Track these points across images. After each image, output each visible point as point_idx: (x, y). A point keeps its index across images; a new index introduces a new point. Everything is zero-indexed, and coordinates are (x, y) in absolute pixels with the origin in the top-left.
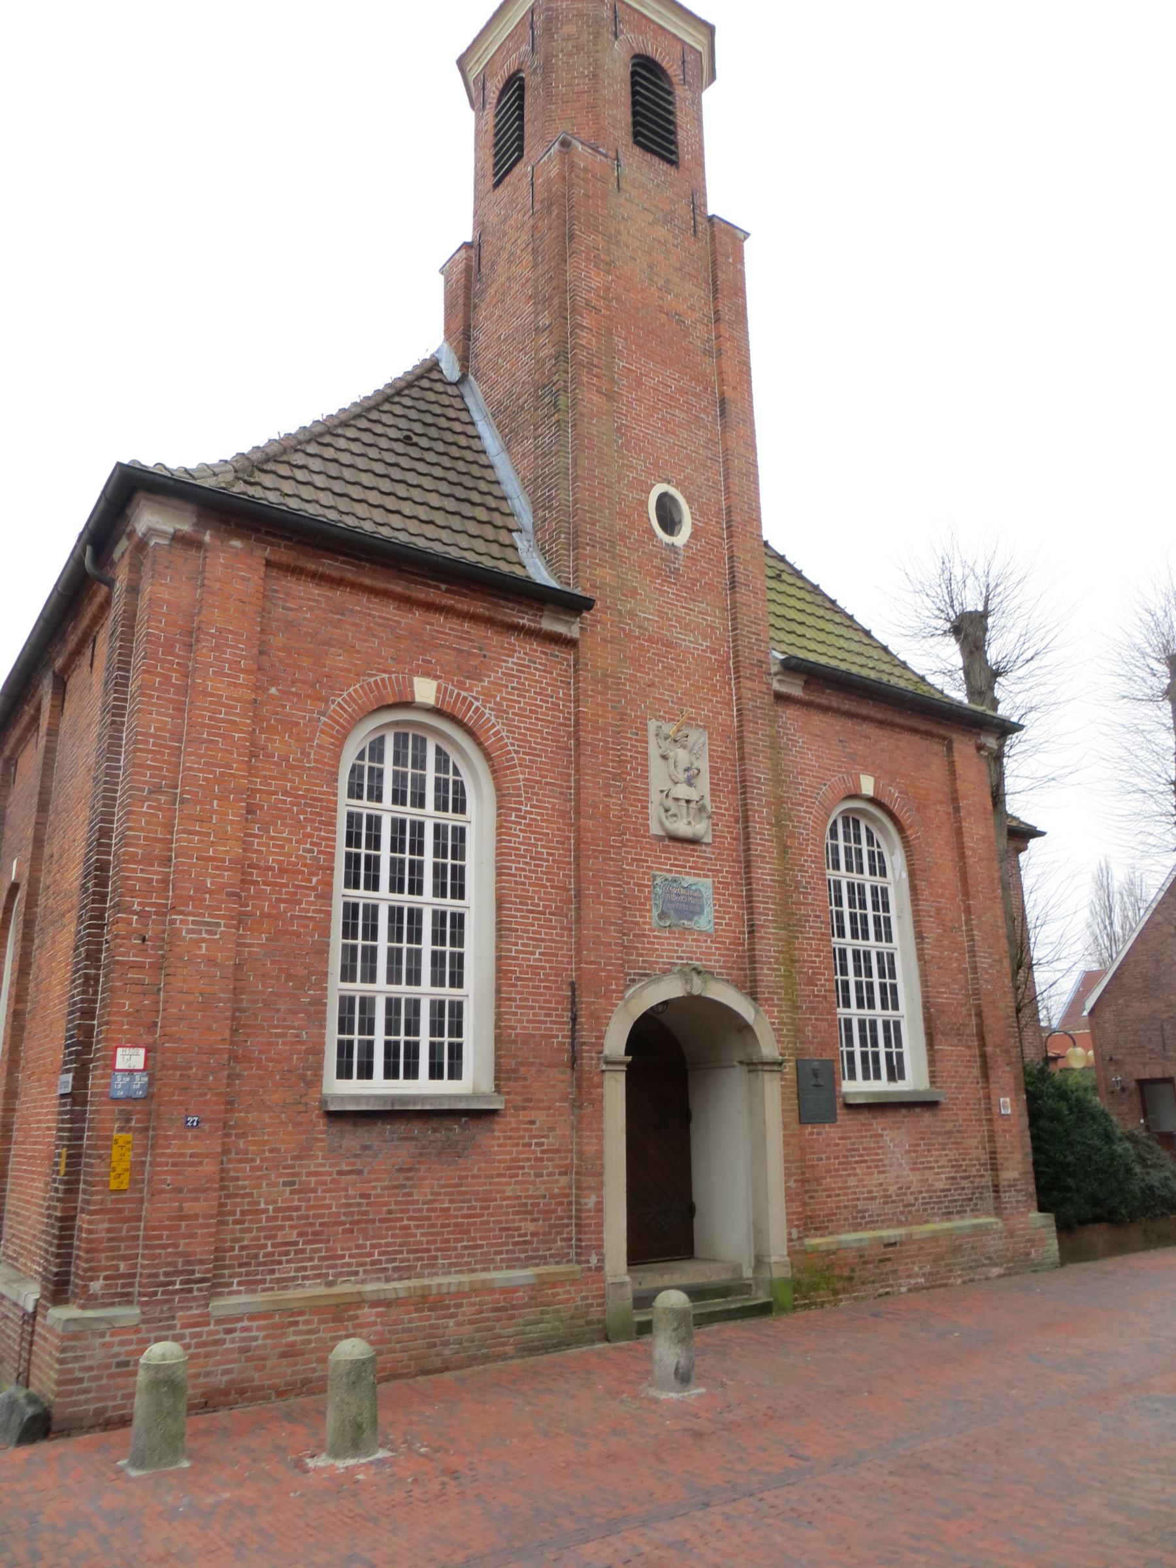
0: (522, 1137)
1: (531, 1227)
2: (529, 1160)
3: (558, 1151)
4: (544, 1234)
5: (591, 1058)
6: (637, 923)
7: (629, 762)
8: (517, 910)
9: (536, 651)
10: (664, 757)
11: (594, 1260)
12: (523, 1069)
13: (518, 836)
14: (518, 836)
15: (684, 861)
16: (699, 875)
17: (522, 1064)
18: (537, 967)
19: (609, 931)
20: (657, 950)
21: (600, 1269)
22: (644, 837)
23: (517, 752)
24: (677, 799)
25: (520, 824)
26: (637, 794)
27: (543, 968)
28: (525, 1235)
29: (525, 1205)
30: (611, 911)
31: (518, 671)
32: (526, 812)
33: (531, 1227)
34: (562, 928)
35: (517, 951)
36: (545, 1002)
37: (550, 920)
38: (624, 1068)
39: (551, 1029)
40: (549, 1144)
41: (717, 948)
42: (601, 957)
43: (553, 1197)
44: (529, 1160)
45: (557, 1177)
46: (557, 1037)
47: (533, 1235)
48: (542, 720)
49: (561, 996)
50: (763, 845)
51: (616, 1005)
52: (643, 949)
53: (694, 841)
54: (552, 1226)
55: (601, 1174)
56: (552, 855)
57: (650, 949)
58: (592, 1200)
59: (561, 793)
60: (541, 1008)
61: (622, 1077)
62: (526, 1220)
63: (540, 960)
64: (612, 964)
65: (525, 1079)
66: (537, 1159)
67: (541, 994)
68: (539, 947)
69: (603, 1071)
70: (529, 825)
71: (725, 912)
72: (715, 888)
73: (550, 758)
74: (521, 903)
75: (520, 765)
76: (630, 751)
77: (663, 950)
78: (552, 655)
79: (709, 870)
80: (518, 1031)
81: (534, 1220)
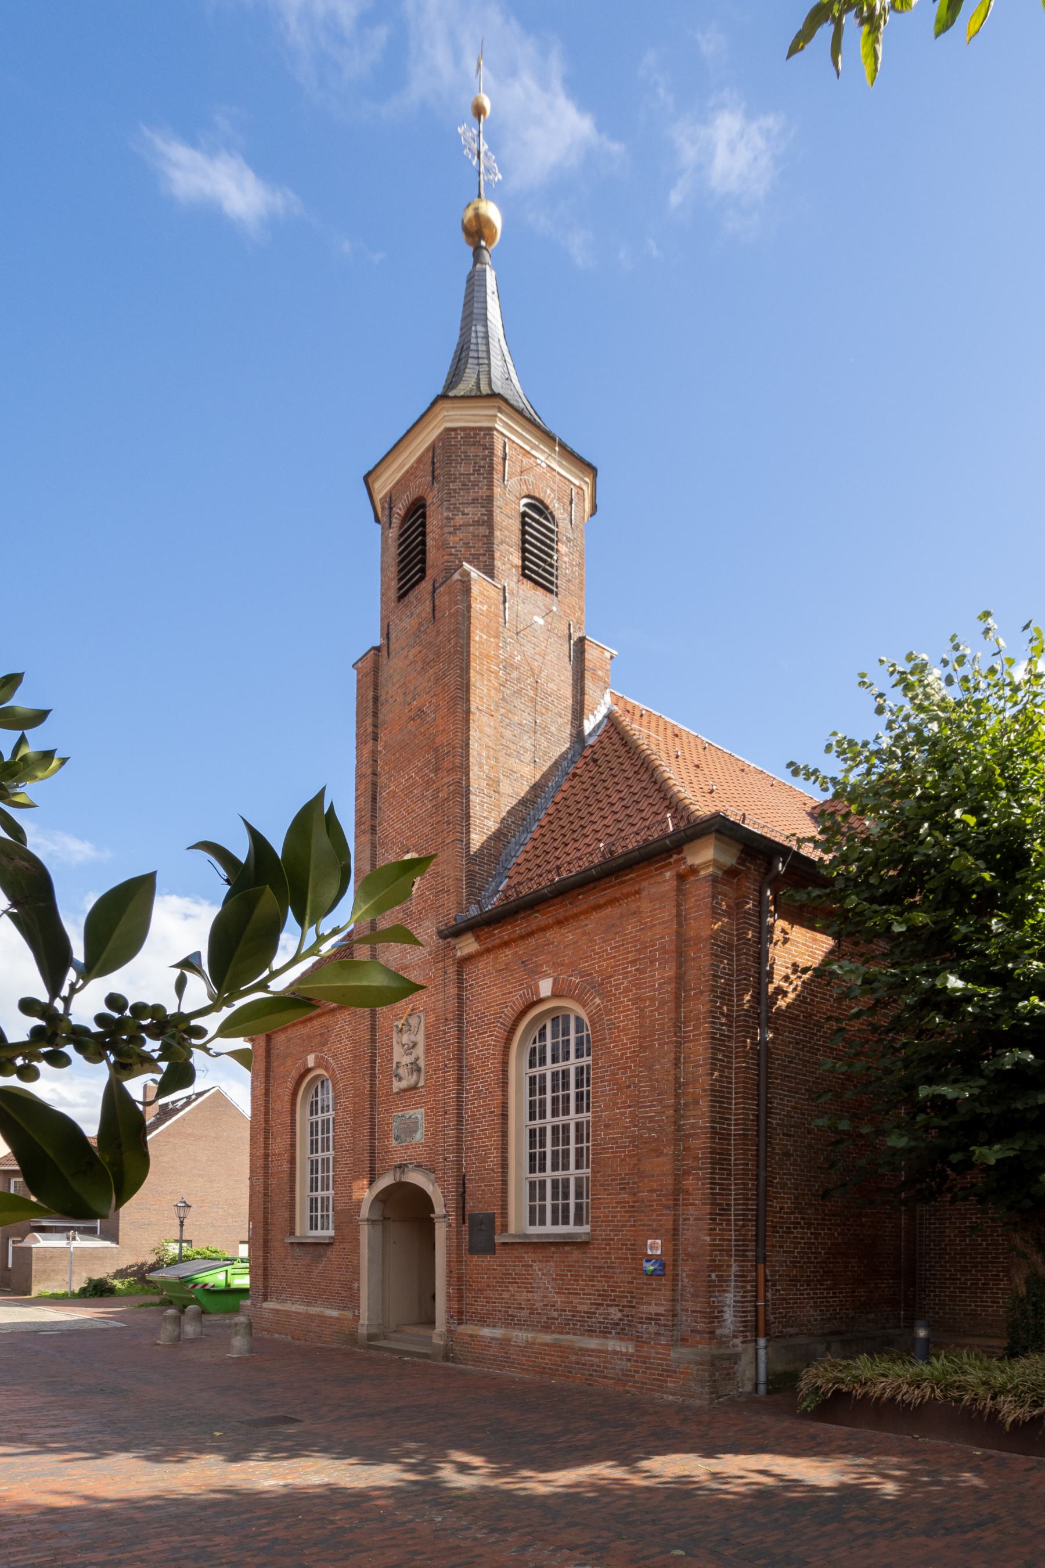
6: (386, 1145)
72: (426, 1113)
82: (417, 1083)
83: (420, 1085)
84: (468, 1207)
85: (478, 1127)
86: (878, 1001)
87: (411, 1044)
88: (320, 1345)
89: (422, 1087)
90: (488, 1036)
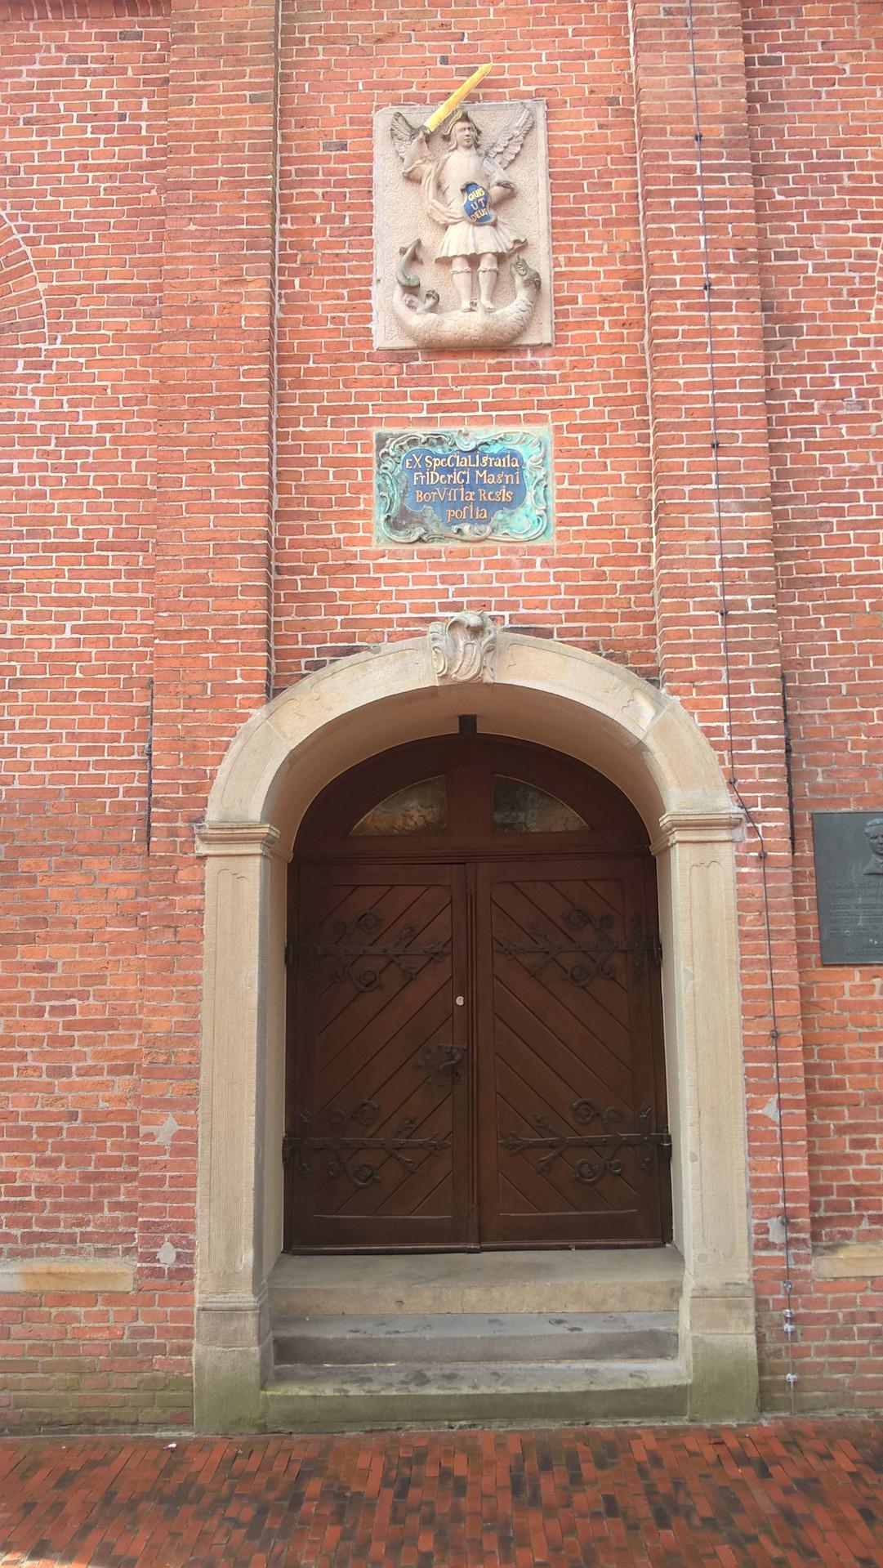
0: (23, 997)
1: (38, 1176)
2: (35, 1041)
3: (109, 1024)
4: (70, 1191)
5: (173, 833)
6: (335, 545)
7: (315, 208)
8: (19, 548)
9: (87, 37)
10: (412, 178)
11: (167, 1256)
12: (24, 863)
13: (32, 403)
14: (32, 403)
15: (469, 394)
16: (515, 420)
17: (23, 851)
18: (64, 657)
19: (229, 564)
20: (386, 595)
21: (183, 1274)
22: (356, 357)
23: (31, 242)
24: (446, 262)
25: (37, 378)
26: (342, 271)
27: (79, 657)
28: (25, 1191)
29: (27, 1131)
30: (236, 522)
31: (41, 86)
32: (51, 353)
33: (38, 1176)
34: (131, 574)
35: (18, 630)
36: (82, 724)
37: (104, 561)
38: (257, 849)
39: (100, 779)
40: (86, 1010)
41: (559, 577)
42: (208, 620)
43: (91, 1117)
44: (35, 1041)
45: (105, 1077)
46: (113, 792)
47: (41, 1191)
48: (99, 168)
49: (123, 710)
50: (692, 320)
51: (244, 718)
52: (344, 597)
53: (500, 346)
54: (88, 1177)
55: (193, 1074)
56: (111, 428)
57: (365, 596)
58: (166, 1129)
59: (138, 303)
60: (73, 737)
61: (257, 862)
62: (28, 1161)
63: (77, 643)
64: (237, 633)
65: (32, 880)
66: (54, 1041)
67: (75, 710)
68: (70, 616)
69: (203, 858)
70: (59, 378)
71: (587, 494)
72: (559, 441)
73: (113, 238)
74: (32, 534)
75: (40, 265)
76: (325, 184)
77: (401, 595)
78: (124, 36)
79: (542, 405)
80: (16, 785)
81: (43, 1163)
82: (523, 330)
83: (531, 339)
84: (804, 787)
85: (839, 512)
86: (857, 908)
87: (495, 191)
88: (31, 1358)
89: (536, 349)
90: (858, 229)
